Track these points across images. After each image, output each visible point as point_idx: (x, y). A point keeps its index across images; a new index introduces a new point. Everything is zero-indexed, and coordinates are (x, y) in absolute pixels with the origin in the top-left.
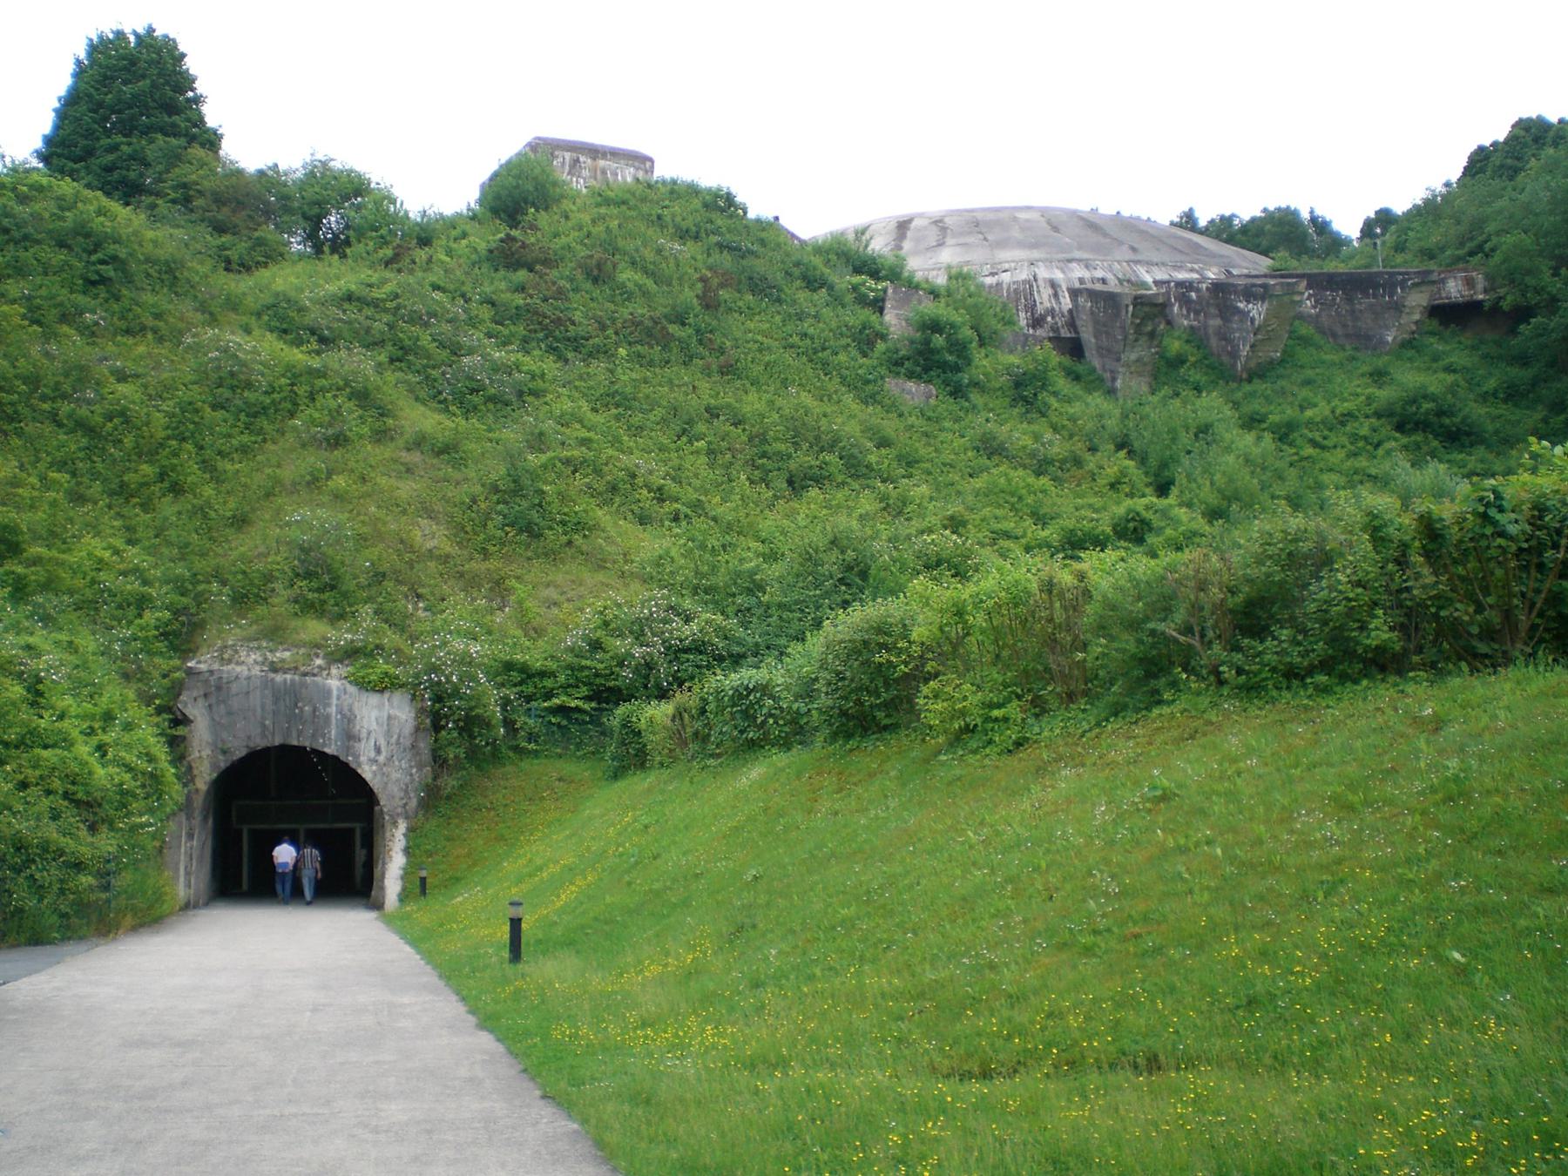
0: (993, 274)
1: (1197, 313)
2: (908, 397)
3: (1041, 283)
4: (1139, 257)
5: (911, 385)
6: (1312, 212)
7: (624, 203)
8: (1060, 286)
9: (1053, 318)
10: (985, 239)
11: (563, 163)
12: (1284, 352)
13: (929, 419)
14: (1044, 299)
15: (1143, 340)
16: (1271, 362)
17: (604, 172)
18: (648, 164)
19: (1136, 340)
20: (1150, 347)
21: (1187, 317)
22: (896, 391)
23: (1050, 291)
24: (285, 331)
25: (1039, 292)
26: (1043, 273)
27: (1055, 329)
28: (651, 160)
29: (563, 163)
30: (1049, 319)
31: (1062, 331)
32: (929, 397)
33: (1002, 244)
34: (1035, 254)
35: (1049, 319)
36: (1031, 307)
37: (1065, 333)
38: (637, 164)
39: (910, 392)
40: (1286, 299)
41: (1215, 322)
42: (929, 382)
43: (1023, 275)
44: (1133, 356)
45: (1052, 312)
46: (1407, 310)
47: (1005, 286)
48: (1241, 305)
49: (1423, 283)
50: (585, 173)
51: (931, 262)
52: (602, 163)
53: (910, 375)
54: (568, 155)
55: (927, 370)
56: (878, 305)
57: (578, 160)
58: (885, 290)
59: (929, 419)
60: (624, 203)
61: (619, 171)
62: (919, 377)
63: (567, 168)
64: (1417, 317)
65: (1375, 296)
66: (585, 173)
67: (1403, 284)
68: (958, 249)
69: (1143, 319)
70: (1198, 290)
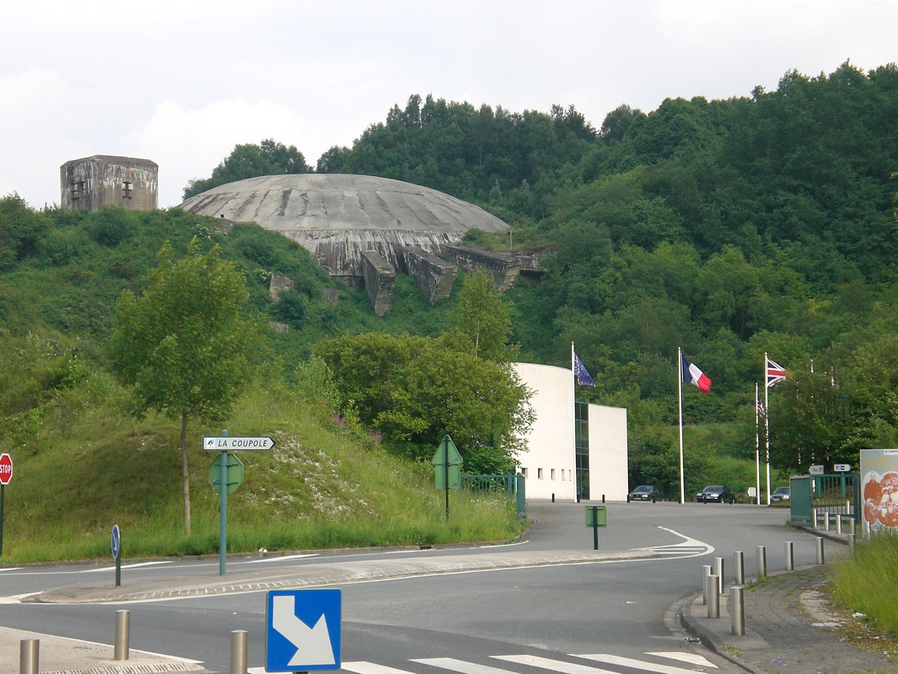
0: (327, 237)
1: (417, 270)
2: (277, 329)
3: (349, 244)
4: (401, 228)
5: (278, 324)
6: (572, 108)
7: (159, 233)
8: (358, 246)
9: (353, 265)
10: (326, 212)
11: (112, 171)
12: (450, 295)
13: (285, 340)
14: (350, 254)
15: (385, 290)
16: (445, 299)
17: (133, 174)
18: (155, 169)
19: (382, 290)
20: (389, 293)
21: (414, 270)
22: (272, 327)
23: (353, 249)
24: (52, 322)
25: (348, 249)
26: (351, 238)
27: (353, 271)
28: (157, 166)
29: (112, 171)
30: (351, 265)
31: (356, 272)
32: (286, 329)
33: (333, 217)
34: (349, 226)
35: (351, 265)
36: (343, 258)
37: (357, 274)
38: (149, 169)
39: (278, 327)
41: (423, 277)
42: (286, 323)
43: (341, 239)
44: (382, 296)
45: (352, 261)
47: (332, 245)
48: (432, 274)
50: (123, 175)
51: (298, 226)
52: (132, 169)
53: (279, 320)
54: (114, 166)
55: (285, 318)
56: (267, 283)
57: (119, 169)
58: (271, 276)
59: (285, 340)
60: (159, 233)
61: (140, 173)
62: (283, 320)
63: (114, 173)
64: (512, 280)
65: (495, 269)
66: (123, 175)
67: (505, 266)
68: (312, 219)
69: (384, 283)
70: (418, 260)
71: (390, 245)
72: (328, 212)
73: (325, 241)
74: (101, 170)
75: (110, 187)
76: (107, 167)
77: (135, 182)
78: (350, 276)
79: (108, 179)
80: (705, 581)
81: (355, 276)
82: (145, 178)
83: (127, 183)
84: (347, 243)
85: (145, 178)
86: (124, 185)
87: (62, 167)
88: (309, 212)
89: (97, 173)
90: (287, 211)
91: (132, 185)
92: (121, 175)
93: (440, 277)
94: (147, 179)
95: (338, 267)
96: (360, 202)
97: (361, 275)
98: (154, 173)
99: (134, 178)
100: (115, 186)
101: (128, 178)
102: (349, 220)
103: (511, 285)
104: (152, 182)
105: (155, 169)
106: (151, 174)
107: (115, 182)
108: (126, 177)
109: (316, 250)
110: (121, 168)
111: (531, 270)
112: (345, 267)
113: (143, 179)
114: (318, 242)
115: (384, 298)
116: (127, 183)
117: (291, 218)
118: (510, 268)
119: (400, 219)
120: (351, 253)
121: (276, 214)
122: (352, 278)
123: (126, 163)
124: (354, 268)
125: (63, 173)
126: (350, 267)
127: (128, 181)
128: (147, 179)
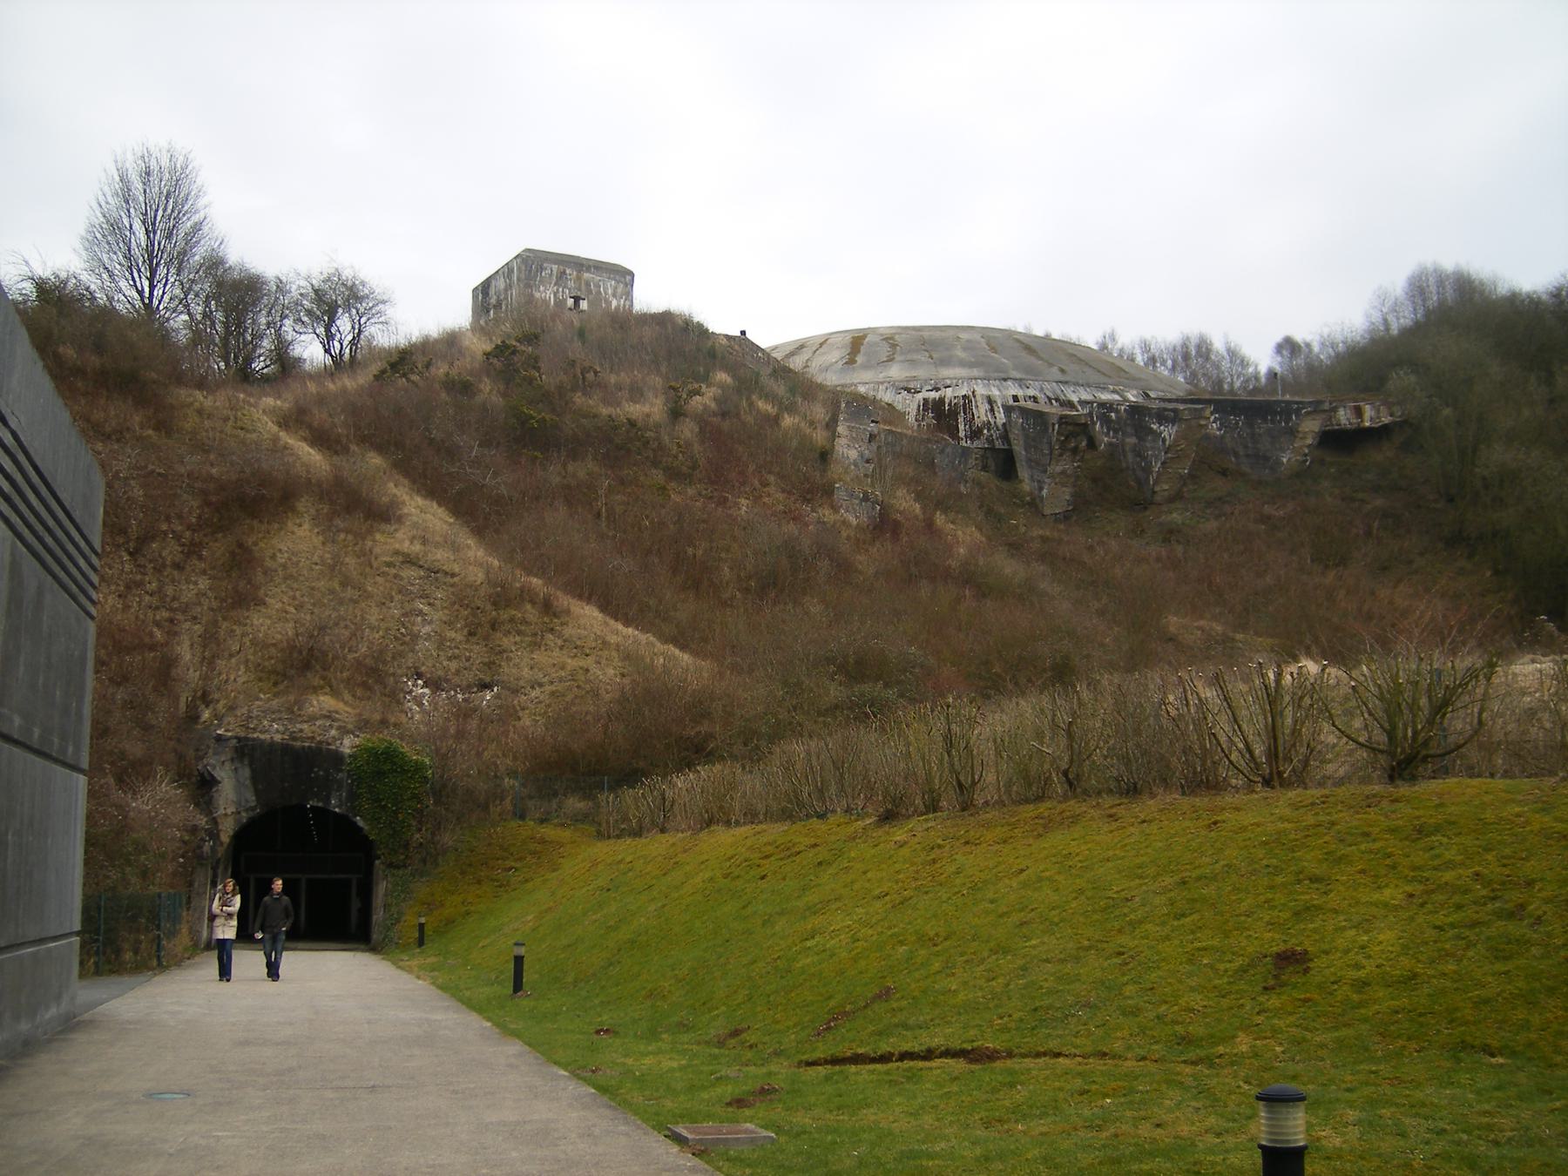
1: (1116, 431)
9: (989, 430)
11: (551, 275)
17: (588, 284)
18: (628, 278)
19: (1061, 455)
21: (1107, 434)
23: (987, 407)
27: (990, 440)
28: (632, 274)
29: (551, 275)
30: (985, 431)
33: (945, 362)
35: (985, 431)
36: (970, 421)
37: (998, 444)
38: (617, 278)
40: (1193, 423)
44: (1059, 469)
46: (1301, 435)
47: (947, 401)
48: (1154, 427)
49: (1315, 411)
50: (571, 284)
51: (881, 375)
52: (586, 275)
54: (555, 267)
57: (564, 272)
61: (601, 284)
64: (1309, 441)
66: (571, 284)
67: (1298, 412)
69: (1067, 437)
70: (1117, 411)
71: (1054, 402)
72: (934, 356)
73: (934, 395)
74: (530, 271)
75: (546, 302)
76: (542, 269)
77: (591, 297)
78: (986, 449)
79: (542, 288)
80: (77, 800)
81: (993, 449)
82: (610, 292)
83: (577, 299)
84: (974, 397)
85: (610, 292)
86: (570, 302)
87: (475, 290)
88: (898, 357)
89: (523, 276)
90: (860, 359)
91: (586, 302)
92: (566, 284)
93: (1175, 428)
94: (614, 295)
95: (962, 434)
96: (988, 344)
97: (1006, 447)
98: (626, 285)
99: (590, 292)
100: (555, 300)
101: (580, 290)
102: (971, 365)
103: (1307, 451)
104: (622, 301)
105: (628, 278)
106: (621, 287)
107: (555, 296)
108: (575, 288)
109: (919, 410)
110: (568, 272)
111: (1336, 427)
112: (975, 434)
113: (606, 293)
114: (920, 396)
115: (1063, 473)
116: (577, 299)
117: (866, 367)
118: (1308, 413)
119: (1064, 367)
120: (982, 411)
121: (841, 363)
122: (989, 454)
123: (574, 263)
124: (992, 436)
125: (475, 297)
126: (983, 434)
127: (579, 294)
128: (614, 295)
